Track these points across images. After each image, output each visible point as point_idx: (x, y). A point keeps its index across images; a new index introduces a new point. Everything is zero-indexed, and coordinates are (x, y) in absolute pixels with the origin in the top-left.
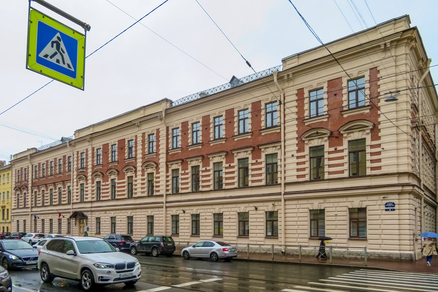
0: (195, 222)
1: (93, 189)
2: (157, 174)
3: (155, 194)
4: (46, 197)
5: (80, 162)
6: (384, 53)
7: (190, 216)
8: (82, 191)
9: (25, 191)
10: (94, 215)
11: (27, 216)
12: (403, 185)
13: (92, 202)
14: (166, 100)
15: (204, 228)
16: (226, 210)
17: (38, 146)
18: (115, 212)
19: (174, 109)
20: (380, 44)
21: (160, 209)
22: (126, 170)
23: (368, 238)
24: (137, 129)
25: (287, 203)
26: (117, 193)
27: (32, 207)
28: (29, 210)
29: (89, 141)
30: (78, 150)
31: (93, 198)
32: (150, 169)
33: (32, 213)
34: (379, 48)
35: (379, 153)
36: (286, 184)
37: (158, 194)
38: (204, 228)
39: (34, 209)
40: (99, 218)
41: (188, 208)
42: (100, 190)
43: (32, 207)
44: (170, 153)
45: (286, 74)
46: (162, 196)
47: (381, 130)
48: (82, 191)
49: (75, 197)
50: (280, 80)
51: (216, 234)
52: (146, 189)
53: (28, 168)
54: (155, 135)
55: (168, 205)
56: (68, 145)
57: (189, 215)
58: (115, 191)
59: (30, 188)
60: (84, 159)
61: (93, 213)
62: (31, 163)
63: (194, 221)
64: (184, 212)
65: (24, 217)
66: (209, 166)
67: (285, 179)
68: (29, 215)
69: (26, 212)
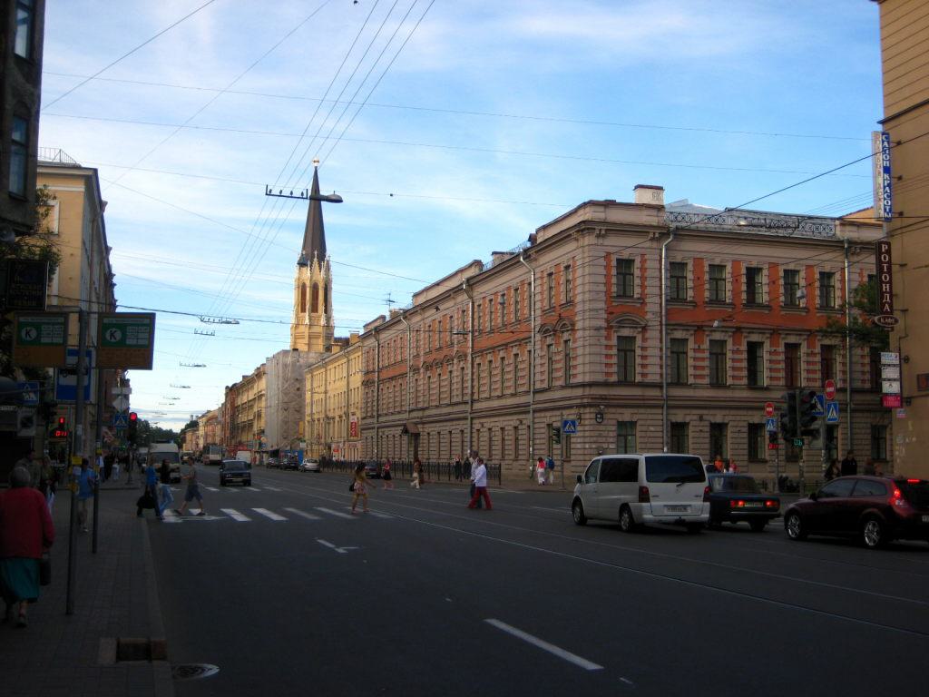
25: (537, 415)
27: (379, 416)
29: (577, 240)
30: (542, 268)
43: (379, 416)
55: (472, 415)
59: (469, 358)
62: (471, 297)
68: (373, 428)
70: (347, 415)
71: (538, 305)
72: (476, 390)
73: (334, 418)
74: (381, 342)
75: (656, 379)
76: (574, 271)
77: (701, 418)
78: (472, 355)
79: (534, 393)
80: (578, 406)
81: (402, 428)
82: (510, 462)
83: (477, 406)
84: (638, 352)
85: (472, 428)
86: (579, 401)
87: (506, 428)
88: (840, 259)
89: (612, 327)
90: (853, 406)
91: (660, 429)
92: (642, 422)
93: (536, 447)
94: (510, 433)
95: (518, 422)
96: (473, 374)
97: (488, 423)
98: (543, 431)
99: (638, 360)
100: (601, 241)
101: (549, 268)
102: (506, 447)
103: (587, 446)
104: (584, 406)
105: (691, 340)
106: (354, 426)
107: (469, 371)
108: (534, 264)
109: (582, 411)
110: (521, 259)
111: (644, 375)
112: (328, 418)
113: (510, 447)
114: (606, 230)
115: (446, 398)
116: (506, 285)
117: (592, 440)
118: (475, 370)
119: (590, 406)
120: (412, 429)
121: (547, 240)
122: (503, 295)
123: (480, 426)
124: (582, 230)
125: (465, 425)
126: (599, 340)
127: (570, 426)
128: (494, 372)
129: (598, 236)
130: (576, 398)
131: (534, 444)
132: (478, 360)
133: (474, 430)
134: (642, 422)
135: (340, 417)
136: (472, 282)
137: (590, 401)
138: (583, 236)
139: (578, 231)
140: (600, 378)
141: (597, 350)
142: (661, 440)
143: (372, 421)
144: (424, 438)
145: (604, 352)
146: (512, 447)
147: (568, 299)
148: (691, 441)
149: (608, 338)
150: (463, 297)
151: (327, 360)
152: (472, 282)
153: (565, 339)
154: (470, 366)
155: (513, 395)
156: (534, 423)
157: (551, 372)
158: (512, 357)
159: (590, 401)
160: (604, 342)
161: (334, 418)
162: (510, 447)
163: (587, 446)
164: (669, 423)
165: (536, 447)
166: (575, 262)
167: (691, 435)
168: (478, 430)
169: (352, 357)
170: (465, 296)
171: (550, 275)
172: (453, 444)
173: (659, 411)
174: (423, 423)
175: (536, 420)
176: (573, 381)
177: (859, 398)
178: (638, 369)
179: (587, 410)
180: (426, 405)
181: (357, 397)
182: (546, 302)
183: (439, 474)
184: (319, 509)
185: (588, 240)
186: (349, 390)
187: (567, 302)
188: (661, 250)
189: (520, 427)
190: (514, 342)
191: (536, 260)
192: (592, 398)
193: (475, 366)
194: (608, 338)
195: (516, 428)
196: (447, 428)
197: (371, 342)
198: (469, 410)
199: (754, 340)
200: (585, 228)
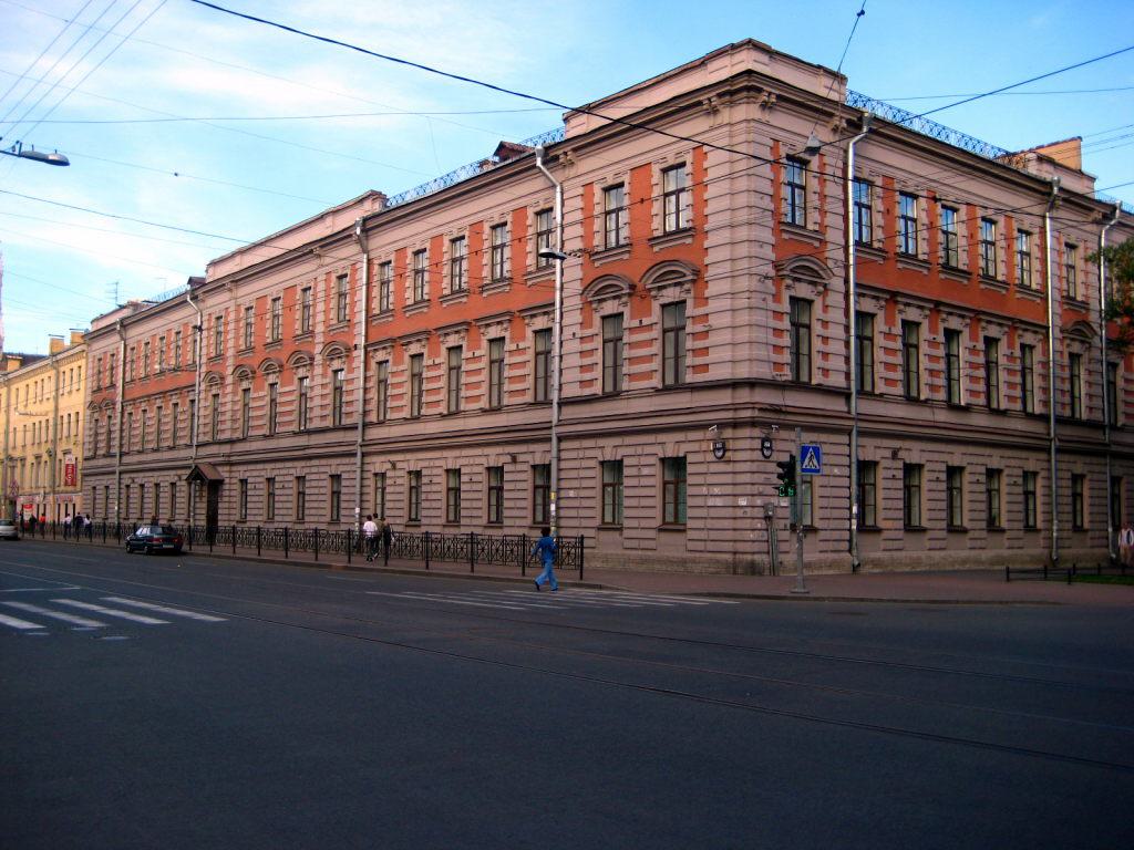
0: (541, 490)
1: (236, 408)
2: (696, 306)
3: (689, 378)
4: (430, 379)
5: (333, 303)
6: (712, 117)
7: (658, 463)
8: (454, 372)
9: (109, 412)
10: (236, 475)
11: (346, 460)
12: (735, 408)
13: (231, 442)
14: (375, 195)
15: (633, 502)
16: (695, 447)
17: (735, 42)
18: (680, 436)
19: (393, 213)
20: (701, 98)
21: (111, 477)
22: (596, 294)
23: (689, 526)
24: (317, 261)
25: (564, 445)
26: (506, 387)
27: (365, 425)
28: (116, 461)
29: (230, 290)
30: (210, 311)
31: (234, 430)
32: (380, 352)
33: (122, 468)
34: (699, 108)
35: (705, 334)
36: (563, 403)
37: (700, 378)
38: (633, 502)
39: (126, 459)
40: (339, 477)
41: (523, 448)
42: (421, 383)
43: (365, 425)
44: (374, 324)
45: (561, 151)
46: (354, 428)
47: (710, 284)
48: (454, 372)
49: (574, 375)
50: (551, 165)
51: (667, 520)
52: (597, 373)
53: (355, 271)
54: (688, 169)
55: (365, 449)
56: (539, 162)
57: (525, 467)
58: (421, 392)
59: (119, 406)
60: (423, 271)
61: (234, 468)
62: (122, 339)
63: (452, 489)
64: (514, 460)
65: (269, 466)
66: (479, 348)
67: (560, 390)
68: (114, 473)
69: (340, 444)
70: (52, 454)
71: (204, 351)
72: (373, 406)
73: (23, 460)
74: (131, 343)
75: (837, 380)
76: (226, 324)
77: (895, 455)
78: (365, 347)
79: (560, 405)
80: (722, 425)
81: (188, 472)
82: (652, 534)
83: (375, 433)
84: (817, 328)
85: (120, 483)
86: (730, 415)
87: (424, 472)
88: (1037, 210)
89: (783, 277)
90: (1058, 443)
91: (846, 471)
92: (633, 461)
93: (563, 503)
94: (166, 489)
95: (176, 478)
96: (122, 423)
97: (140, 478)
98: (261, 486)
99: (817, 344)
100: (766, 116)
101: (98, 354)
102: (131, 506)
103: (743, 502)
104: (736, 425)
105: (881, 316)
106: (71, 469)
107: (118, 420)
108: (202, 305)
109: (728, 433)
110: (188, 299)
111: (826, 372)
112: (11, 459)
113: (166, 506)
114: (779, 97)
115: (152, 440)
116: (103, 350)
117: (755, 489)
118: (124, 420)
119: (753, 423)
120: (210, 474)
121: (647, 109)
122: (162, 339)
123: (130, 481)
124: (731, 93)
125: (113, 481)
126: (764, 300)
127: (811, 459)
128: (181, 417)
129: (765, 106)
130: (724, 408)
131: (559, 499)
132: (129, 409)
133: (122, 486)
134: (633, 461)
135: (38, 457)
136: (371, 224)
137: (756, 413)
138: (732, 104)
139: (232, 282)
140: (765, 372)
141: (759, 317)
142: (846, 492)
143: (108, 456)
144: (231, 491)
145: (773, 323)
146: (103, 506)
147: (275, 336)
148: (881, 494)
149: (777, 298)
150: (350, 250)
151: (10, 376)
152: (371, 224)
153: (271, 382)
154: (119, 415)
155: (171, 448)
156: (559, 459)
157: (96, 442)
158: (188, 403)
159: (756, 413)
160: (772, 305)
161: (23, 460)
162: (166, 506)
163: (743, 502)
164: (8, 501)
165: (563, 503)
166: (316, 285)
167: (881, 484)
168: (128, 486)
169: (66, 368)
170: (117, 337)
171: (100, 360)
172: (145, 501)
173: (845, 439)
174: (231, 464)
175: (564, 455)
176: (311, 426)
177: (1068, 431)
178: (817, 361)
179: (746, 432)
180: (238, 435)
181: (82, 429)
182: (212, 349)
183: (54, 533)
184: (110, 599)
185: (745, 111)
186: (58, 419)
187: (304, 333)
188: (846, 151)
189: (178, 484)
190: (143, 397)
191: (203, 301)
192: (761, 409)
193: (126, 415)
194: (777, 298)
195: (173, 484)
196: (90, 483)
197: (112, 343)
198: (360, 440)
199: (952, 327)
200: (744, 87)
